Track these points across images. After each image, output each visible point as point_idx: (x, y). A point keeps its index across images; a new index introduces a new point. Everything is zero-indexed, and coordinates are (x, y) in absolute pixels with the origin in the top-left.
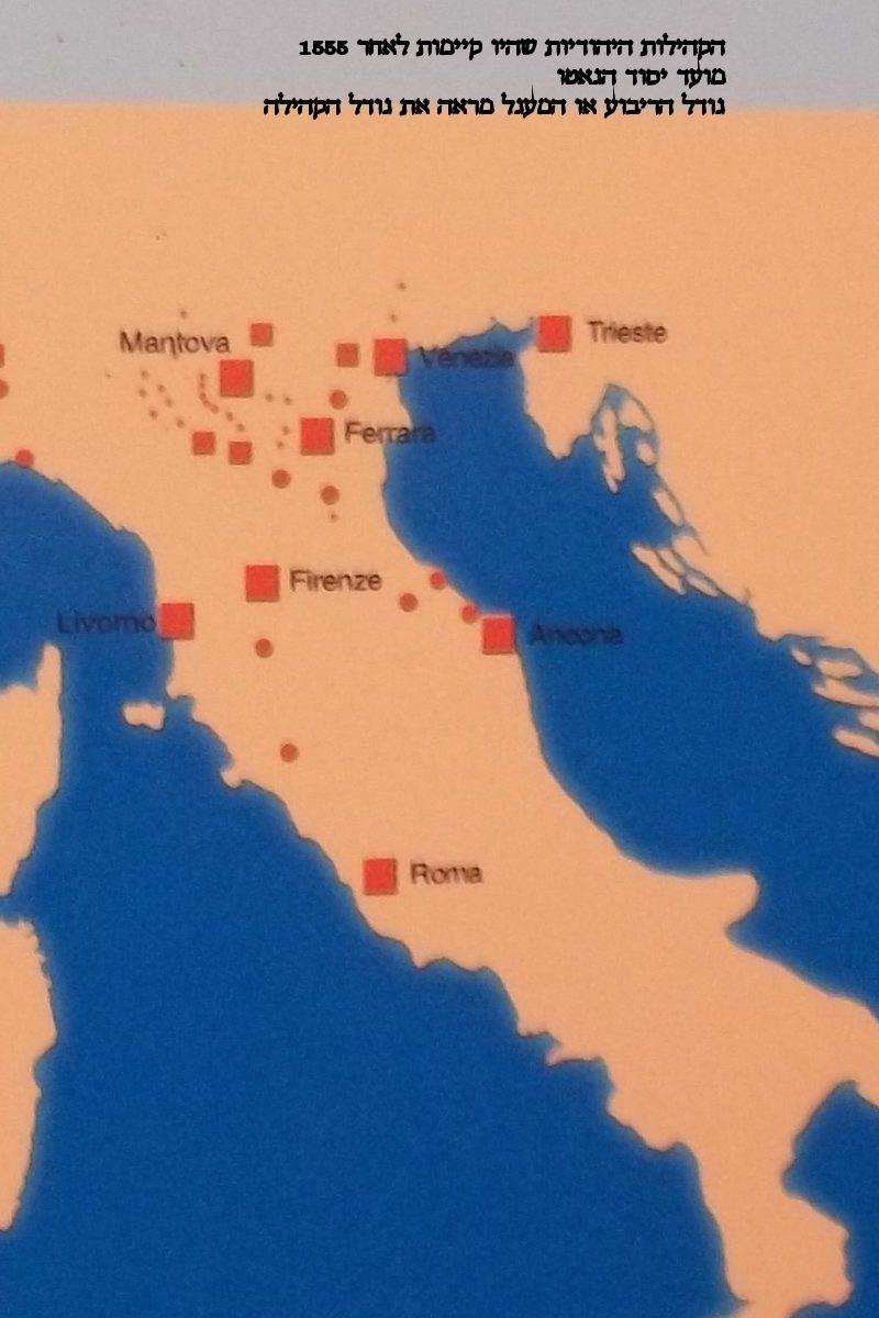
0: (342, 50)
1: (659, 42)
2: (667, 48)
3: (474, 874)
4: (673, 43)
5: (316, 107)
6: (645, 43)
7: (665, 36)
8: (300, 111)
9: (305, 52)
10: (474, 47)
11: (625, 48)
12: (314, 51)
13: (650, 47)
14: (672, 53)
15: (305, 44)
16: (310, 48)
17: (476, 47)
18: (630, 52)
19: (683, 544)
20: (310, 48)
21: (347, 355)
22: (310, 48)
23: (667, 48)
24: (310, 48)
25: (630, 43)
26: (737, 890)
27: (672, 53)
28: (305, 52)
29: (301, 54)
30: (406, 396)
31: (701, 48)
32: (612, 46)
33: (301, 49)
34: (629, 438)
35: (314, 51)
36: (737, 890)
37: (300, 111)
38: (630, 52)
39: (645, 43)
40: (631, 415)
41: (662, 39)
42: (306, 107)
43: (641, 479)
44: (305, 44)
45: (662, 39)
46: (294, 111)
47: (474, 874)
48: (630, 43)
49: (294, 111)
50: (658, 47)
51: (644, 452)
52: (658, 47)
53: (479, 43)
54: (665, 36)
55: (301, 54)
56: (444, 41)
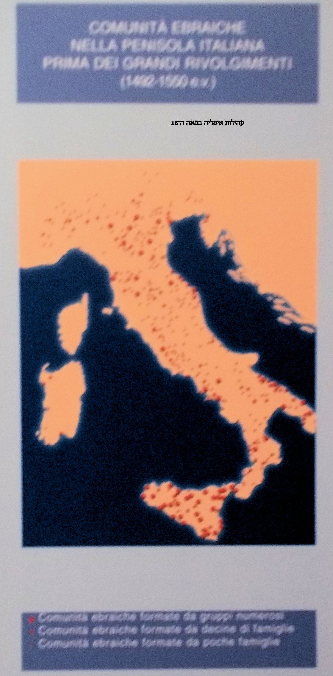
0: (176, 124)
1: (230, 121)
2: (232, 123)
3: (241, 123)
4: (234, 122)
5: (241, 123)
6: (226, 122)
7: (232, 120)
8: (237, 124)
9: (173, 124)
10: (221, 123)
11: (182, 123)
12: (175, 124)
13: (227, 123)
14: (233, 124)
15: (173, 122)
16: (174, 123)
17: (242, 123)
18: (184, 124)
19: (240, 270)
20: (174, 123)
21: (128, 272)
22: (174, 123)
23: (232, 123)
24: (174, 123)
25: (183, 122)
26: (253, 358)
27: (233, 124)
28: (173, 124)
29: (172, 125)
30: (64, 442)
31: (241, 123)
32: (208, 123)
33: (172, 123)
34: (227, 243)
35: (175, 124)
36: (253, 358)
37: (237, 124)
38: (184, 124)
39: (226, 122)
40: (227, 237)
41: (231, 121)
42: (238, 123)
43: (230, 254)
44: (173, 122)
45: (231, 121)
46: (235, 124)
47: (241, 123)
48: (183, 122)
49: (235, 124)
50: (230, 123)
51: (231, 247)
52: (230, 123)
53: (243, 122)
54: (232, 120)
55: (172, 125)
56: (195, 121)
